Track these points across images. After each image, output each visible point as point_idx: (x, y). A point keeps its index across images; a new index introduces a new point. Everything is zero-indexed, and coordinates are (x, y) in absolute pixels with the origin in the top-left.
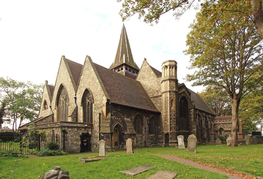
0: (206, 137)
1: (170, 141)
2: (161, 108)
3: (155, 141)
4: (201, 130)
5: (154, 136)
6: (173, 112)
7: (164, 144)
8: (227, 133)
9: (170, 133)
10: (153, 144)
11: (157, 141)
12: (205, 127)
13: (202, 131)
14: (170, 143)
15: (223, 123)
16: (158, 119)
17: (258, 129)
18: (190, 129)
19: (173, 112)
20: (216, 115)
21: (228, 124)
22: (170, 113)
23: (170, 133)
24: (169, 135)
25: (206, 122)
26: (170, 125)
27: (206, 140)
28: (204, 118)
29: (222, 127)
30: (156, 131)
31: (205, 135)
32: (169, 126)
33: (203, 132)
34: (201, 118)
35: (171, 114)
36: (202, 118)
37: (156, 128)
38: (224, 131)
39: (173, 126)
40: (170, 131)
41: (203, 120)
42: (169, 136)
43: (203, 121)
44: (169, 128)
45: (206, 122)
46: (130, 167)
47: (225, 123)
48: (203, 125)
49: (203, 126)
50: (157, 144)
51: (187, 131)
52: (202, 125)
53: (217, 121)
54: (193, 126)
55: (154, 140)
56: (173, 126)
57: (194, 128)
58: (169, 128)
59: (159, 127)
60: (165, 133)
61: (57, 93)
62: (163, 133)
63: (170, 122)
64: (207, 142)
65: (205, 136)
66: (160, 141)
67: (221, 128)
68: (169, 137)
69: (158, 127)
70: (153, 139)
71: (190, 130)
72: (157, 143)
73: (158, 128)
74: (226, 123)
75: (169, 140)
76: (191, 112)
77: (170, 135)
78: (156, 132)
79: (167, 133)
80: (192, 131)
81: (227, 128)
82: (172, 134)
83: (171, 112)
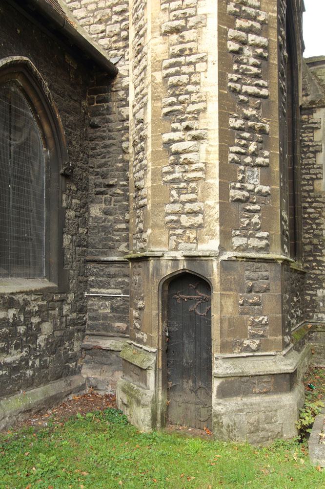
1: (221, 367)
2: (116, 28)
3: (54, 346)
5: (42, 293)
6: (249, 30)
7: (154, 401)
9: (226, 266)
10: (30, 384)
11: (77, 347)
14: (224, 393)
16: (94, 126)
19: (249, 30)
22: (222, 35)
23: (226, 266)
24: (205, 284)
26: (227, 171)
30: (67, 240)
32: (214, 181)
35: (233, 46)
37: (71, 214)
39: (254, 182)
40: (225, 236)
42: (208, 301)
44: (213, 202)
46: (35, 349)
50: (77, 380)
55: (41, 340)
56: (254, 182)
58: (216, 212)
59: (95, 211)
60: (167, 271)
61: (216, 390)
62: (145, 259)
63: (227, 135)
68: (215, 316)
69: (85, 206)
70: (33, 334)
71: (310, 253)
72: (77, 371)
73: (83, 217)
75: (216, 354)
76: (314, 129)
77: (226, 286)
78: (61, 251)
79: (183, 266)
82: (248, 273)
83: (232, 25)
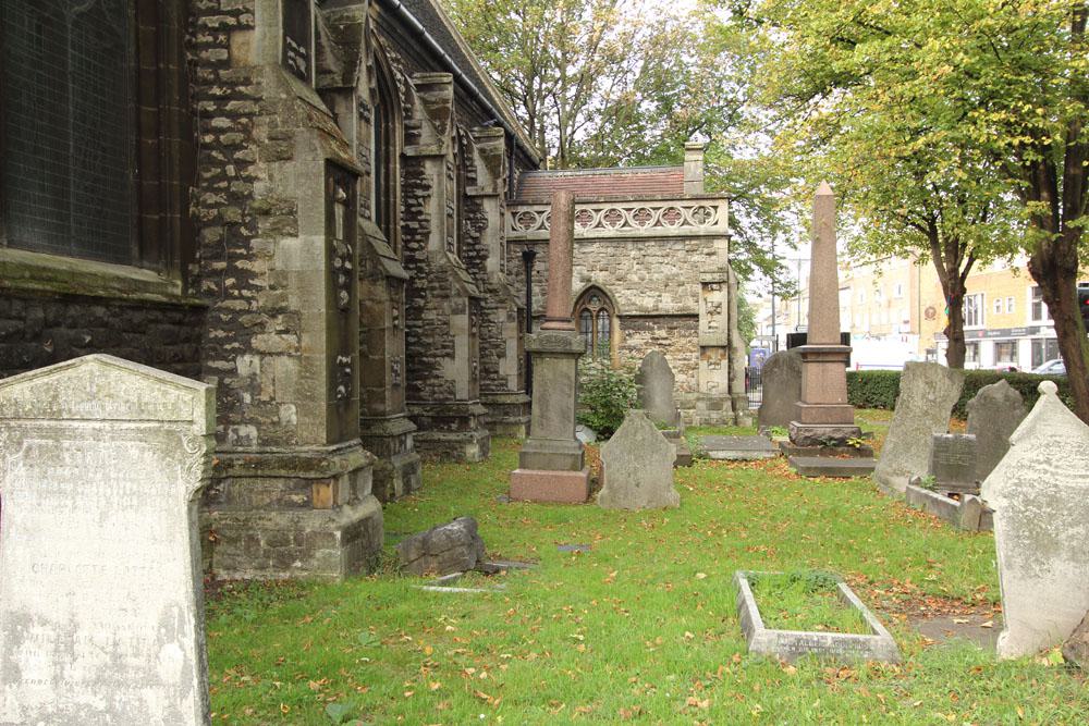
0: (463, 390)
4: (410, 293)
8: (647, 336)
12: (453, 257)
13: (420, 310)
15: (609, 231)
17: (1014, 357)
18: (211, 235)
20: (543, 160)
21: (653, 248)
25: (469, 205)
27: (464, 421)
28: (446, 139)
29: (599, 277)
31: (452, 356)
33: (430, 315)
34: (411, 139)
36: (426, 134)
38: (616, 322)
41: (438, 158)
43: (430, 169)
45: (469, 205)
47: (627, 232)
48: (434, 226)
49: (434, 242)
51: (146, 275)
52: (416, 234)
53: (678, 205)
54: (266, 181)
57: (284, 217)
64: (473, 450)
65: (456, 371)
66: (238, 251)
67: (593, 291)
71: (218, 252)
74: (637, 240)
80: (244, 278)
81: (643, 287)
